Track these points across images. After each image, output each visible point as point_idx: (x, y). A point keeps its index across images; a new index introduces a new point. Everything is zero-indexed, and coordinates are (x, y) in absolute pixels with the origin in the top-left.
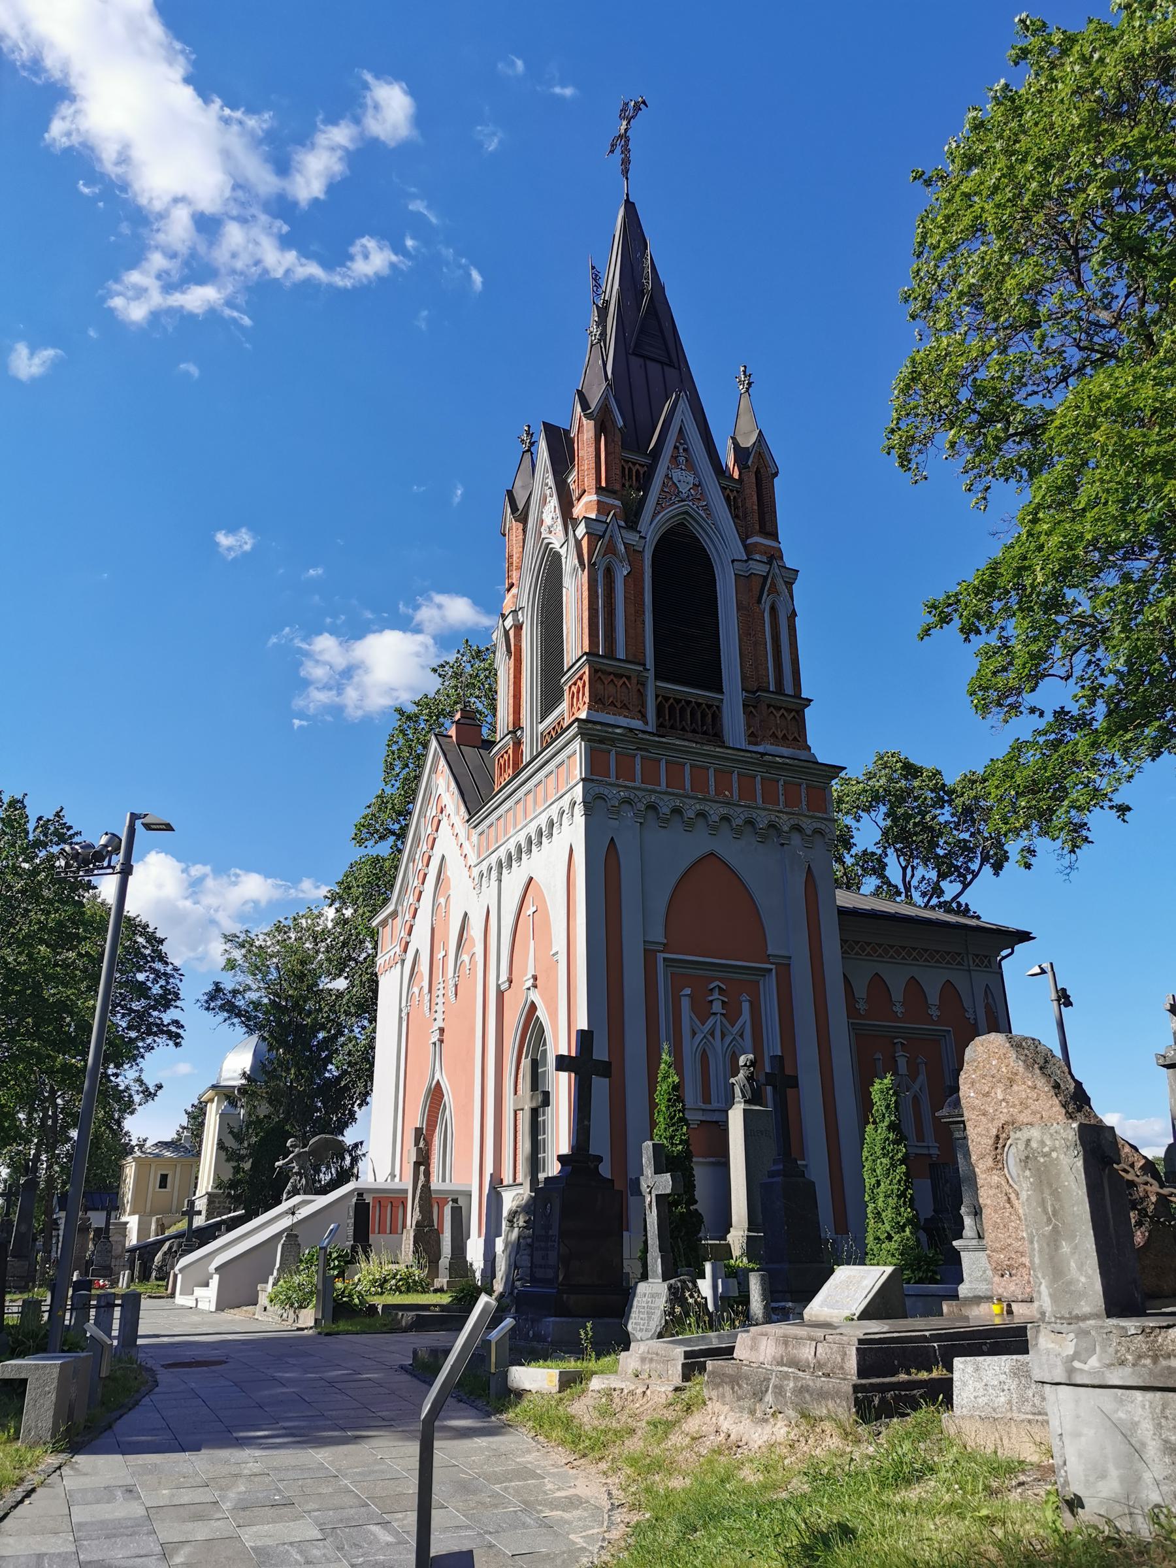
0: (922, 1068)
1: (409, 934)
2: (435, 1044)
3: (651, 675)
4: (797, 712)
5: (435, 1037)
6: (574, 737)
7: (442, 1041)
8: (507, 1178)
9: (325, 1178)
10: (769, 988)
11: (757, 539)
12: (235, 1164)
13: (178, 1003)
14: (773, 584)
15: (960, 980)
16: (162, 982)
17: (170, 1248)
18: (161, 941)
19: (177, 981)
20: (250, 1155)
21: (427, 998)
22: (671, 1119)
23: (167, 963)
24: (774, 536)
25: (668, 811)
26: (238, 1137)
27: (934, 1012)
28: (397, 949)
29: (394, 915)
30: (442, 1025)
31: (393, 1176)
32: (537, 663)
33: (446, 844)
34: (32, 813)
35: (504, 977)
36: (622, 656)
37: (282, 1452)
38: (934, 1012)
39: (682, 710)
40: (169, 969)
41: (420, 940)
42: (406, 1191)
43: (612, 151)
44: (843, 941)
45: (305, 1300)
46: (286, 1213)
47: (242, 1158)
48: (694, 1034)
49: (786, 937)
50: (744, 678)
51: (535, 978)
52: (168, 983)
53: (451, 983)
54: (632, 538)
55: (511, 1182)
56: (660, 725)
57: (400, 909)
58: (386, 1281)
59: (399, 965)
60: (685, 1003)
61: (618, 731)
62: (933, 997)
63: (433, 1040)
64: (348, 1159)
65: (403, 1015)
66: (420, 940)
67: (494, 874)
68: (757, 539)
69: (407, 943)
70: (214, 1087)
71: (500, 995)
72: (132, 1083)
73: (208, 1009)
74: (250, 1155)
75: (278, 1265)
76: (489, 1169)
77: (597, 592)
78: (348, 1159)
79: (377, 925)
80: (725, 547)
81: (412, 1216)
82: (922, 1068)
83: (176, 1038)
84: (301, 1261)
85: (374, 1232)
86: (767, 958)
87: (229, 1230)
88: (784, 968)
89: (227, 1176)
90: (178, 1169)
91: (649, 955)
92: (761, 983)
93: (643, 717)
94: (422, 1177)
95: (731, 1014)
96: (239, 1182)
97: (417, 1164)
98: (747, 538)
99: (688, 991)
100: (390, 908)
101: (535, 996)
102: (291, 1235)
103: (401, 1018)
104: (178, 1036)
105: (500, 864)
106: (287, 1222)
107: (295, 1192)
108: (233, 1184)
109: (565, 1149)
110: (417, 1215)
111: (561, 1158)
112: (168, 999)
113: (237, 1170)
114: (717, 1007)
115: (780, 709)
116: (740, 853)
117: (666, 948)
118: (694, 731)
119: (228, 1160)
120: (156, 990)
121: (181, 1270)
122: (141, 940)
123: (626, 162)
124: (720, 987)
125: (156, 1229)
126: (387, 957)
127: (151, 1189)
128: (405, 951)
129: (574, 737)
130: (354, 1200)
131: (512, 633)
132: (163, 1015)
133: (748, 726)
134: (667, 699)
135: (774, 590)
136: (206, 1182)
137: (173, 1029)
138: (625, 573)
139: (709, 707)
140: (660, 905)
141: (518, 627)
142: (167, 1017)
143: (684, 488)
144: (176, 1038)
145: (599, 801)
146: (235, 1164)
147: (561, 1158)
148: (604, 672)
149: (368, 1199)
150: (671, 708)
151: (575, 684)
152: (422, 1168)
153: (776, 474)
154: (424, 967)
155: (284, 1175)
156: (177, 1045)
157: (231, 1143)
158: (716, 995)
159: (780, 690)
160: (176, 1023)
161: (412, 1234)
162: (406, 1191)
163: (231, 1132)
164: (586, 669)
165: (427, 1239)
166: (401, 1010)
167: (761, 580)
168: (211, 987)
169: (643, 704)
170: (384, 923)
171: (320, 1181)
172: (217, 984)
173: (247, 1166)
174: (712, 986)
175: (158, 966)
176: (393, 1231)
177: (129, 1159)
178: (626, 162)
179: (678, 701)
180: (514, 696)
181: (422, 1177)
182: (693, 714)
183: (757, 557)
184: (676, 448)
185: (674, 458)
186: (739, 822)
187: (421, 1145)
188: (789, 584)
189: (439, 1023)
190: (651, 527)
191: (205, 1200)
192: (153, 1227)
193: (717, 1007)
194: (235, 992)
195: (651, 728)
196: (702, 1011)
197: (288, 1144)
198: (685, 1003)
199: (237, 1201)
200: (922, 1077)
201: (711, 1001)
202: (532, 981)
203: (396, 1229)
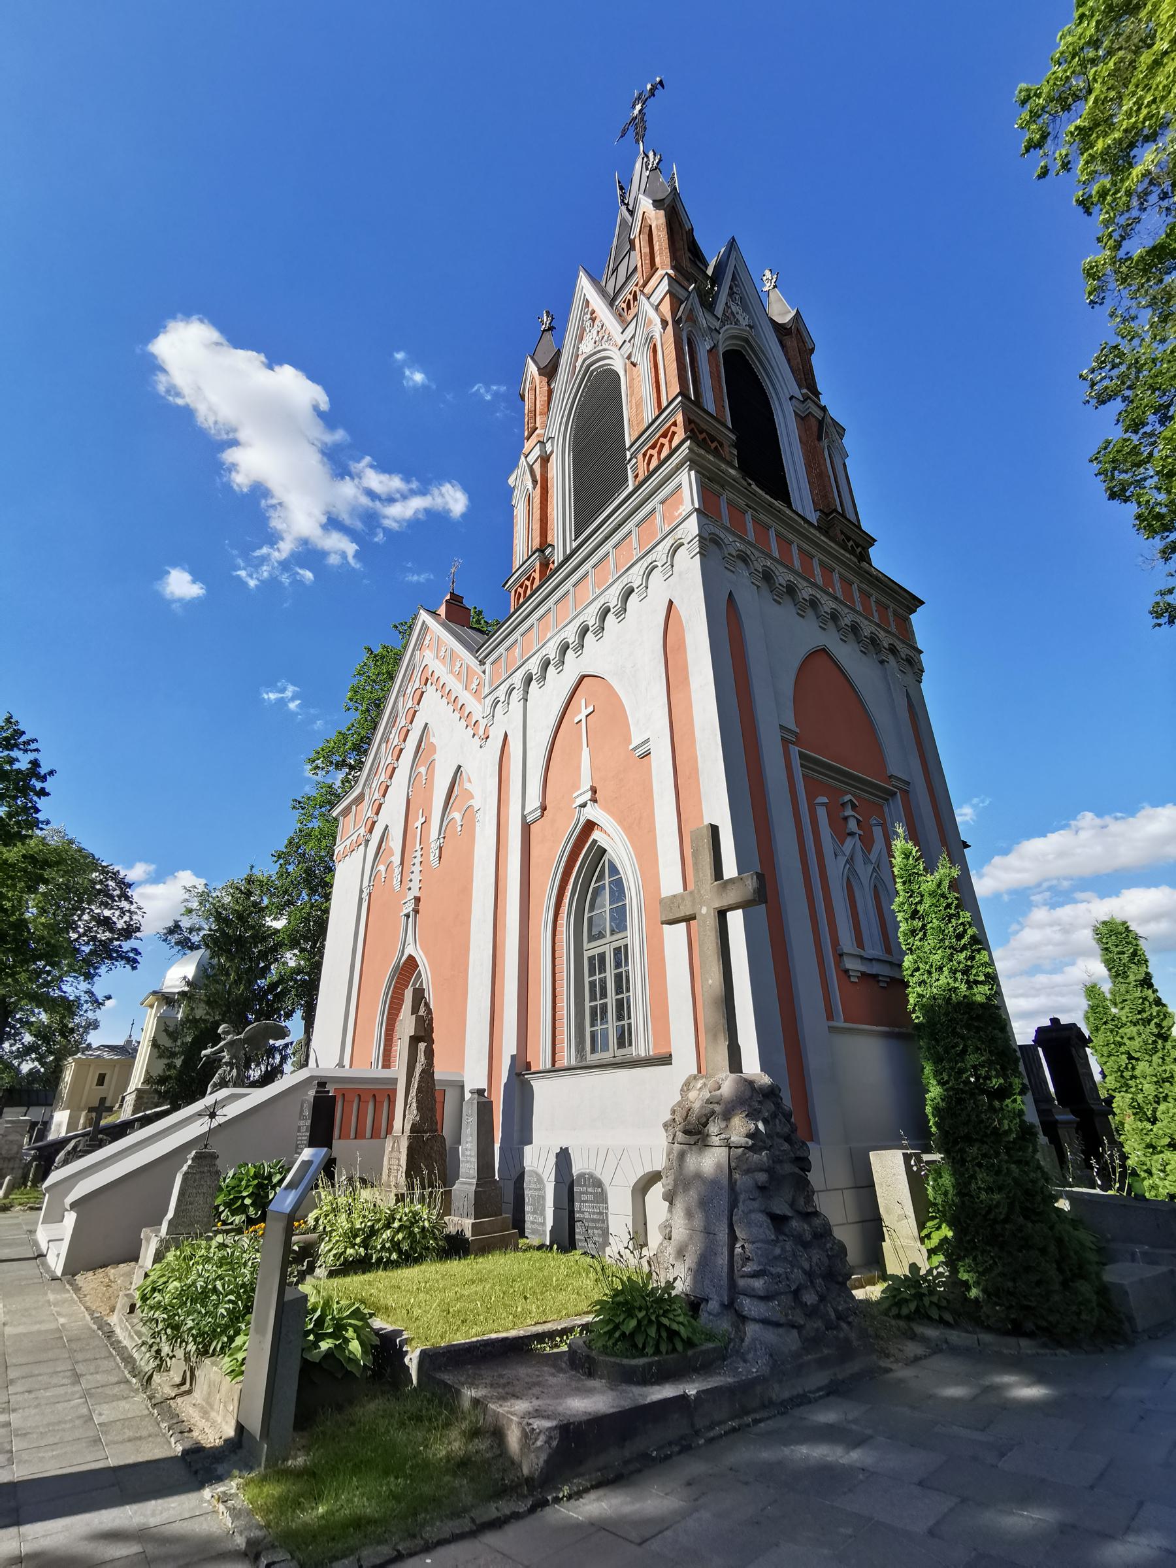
1: (377, 814)
2: (408, 916)
4: (863, 548)
5: (409, 908)
6: (678, 468)
7: (416, 912)
8: (541, 1058)
9: (255, 1073)
12: (166, 1061)
13: (138, 934)
16: (126, 918)
17: (75, 1148)
18: (129, 886)
19: (140, 918)
20: (182, 1053)
21: (397, 871)
22: (959, 937)
23: (131, 903)
26: (173, 1035)
28: (362, 831)
29: (360, 799)
30: (418, 895)
31: (341, 1065)
32: (569, 484)
34: (41, 803)
35: (534, 802)
40: (133, 908)
41: (392, 814)
42: (395, 1081)
45: (214, 1335)
46: (200, 1114)
47: (173, 1055)
51: (594, 790)
52: (131, 919)
53: (434, 846)
55: (549, 1066)
57: (367, 791)
58: (373, 1232)
59: (362, 848)
60: (822, 813)
63: (405, 912)
64: (278, 1057)
65: (365, 896)
66: (392, 814)
67: (517, 695)
69: (374, 823)
70: (155, 993)
71: (526, 827)
72: (82, 994)
73: (165, 940)
74: (182, 1053)
75: (170, 1214)
76: (509, 1047)
77: (682, 349)
78: (278, 1057)
79: (339, 814)
81: (403, 1118)
83: (133, 963)
84: (221, 1189)
85: (343, 1136)
87: (142, 1127)
89: (158, 1071)
90: (117, 1069)
92: (886, 808)
94: (421, 1057)
96: (169, 1077)
97: (415, 1040)
100: (357, 792)
101: (592, 813)
102: (204, 1157)
103: (361, 899)
104: (135, 961)
105: (528, 680)
106: (200, 1127)
107: (223, 1084)
108: (162, 1080)
110: (413, 1115)
112: (129, 931)
113: (170, 1066)
114: (852, 825)
116: (846, 654)
119: (160, 1057)
120: (120, 924)
121: (47, 1189)
122: (111, 883)
125: (85, 1123)
126: (348, 843)
127: (87, 1088)
128: (371, 831)
129: (678, 468)
130: (312, 1093)
131: (537, 468)
132: (123, 944)
136: (137, 1079)
137: (131, 955)
138: (708, 348)
140: (787, 684)
141: (545, 459)
142: (126, 946)
144: (133, 963)
146: (166, 1061)
149: (331, 1089)
152: (422, 1046)
153: (812, 351)
154: (395, 843)
155: (213, 1064)
156: (134, 968)
157: (166, 1042)
158: (849, 812)
160: (135, 950)
161: (404, 1144)
162: (395, 1081)
163: (166, 1030)
164: (680, 418)
165: (429, 1156)
166: (361, 891)
168: (171, 924)
170: (346, 812)
171: (248, 1078)
172: (176, 922)
173: (178, 1062)
175: (124, 904)
176: (375, 1134)
177: (70, 1059)
180: (541, 520)
181: (421, 1057)
187: (422, 1012)
189: (416, 892)
191: (134, 1096)
192: (82, 1121)
194: (191, 930)
197: (220, 1031)
198: (822, 813)
199: (163, 1097)
202: (590, 793)
203: (381, 1130)
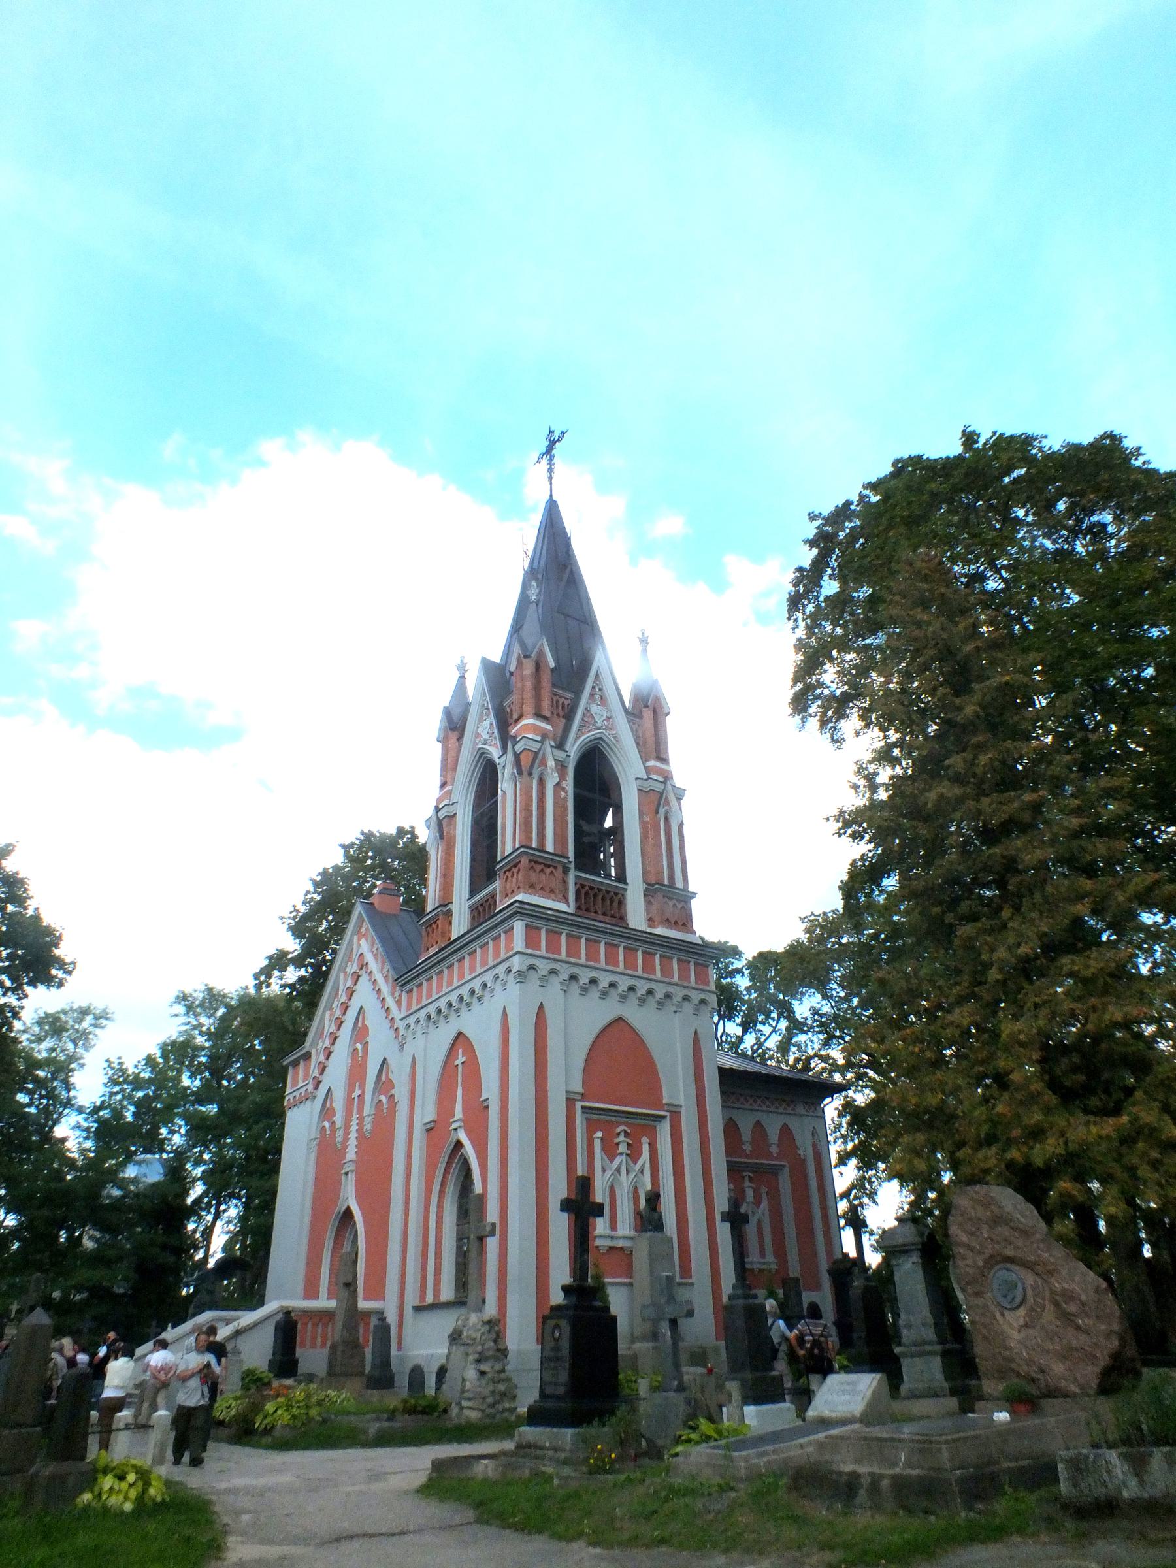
0: (765, 1197)
3: (572, 866)
10: (664, 1132)
11: (652, 763)
14: (667, 799)
15: (794, 1124)
24: (665, 760)
25: (587, 981)
27: (774, 1150)
33: (364, 996)
36: (534, 846)
37: (921, 1401)
38: (774, 1150)
39: (595, 896)
43: (539, 461)
44: (722, 1093)
48: (604, 1171)
49: (677, 1087)
50: (645, 872)
54: (561, 755)
56: (578, 908)
60: (598, 1145)
61: (550, 912)
62: (773, 1136)
68: (652, 763)
80: (629, 769)
82: (765, 1197)
86: (661, 1107)
88: (675, 1115)
91: (570, 1102)
93: (566, 900)
95: (634, 1155)
98: (647, 761)
99: (599, 1134)
109: (567, 1279)
111: (565, 1289)
114: (623, 1148)
115: (671, 898)
116: (642, 1018)
117: (583, 1097)
118: (604, 914)
123: (551, 471)
124: (625, 1132)
133: (648, 911)
134: (583, 886)
135: (667, 802)
139: (616, 894)
143: (599, 721)
145: (532, 971)
147: (565, 1289)
148: (536, 862)
150: (587, 894)
151: (509, 870)
158: (622, 1137)
159: (672, 884)
167: (657, 796)
169: (566, 889)
174: (618, 1130)
178: (551, 471)
179: (592, 888)
182: (603, 899)
183: (654, 777)
184: (593, 687)
185: (592, 695)
186: (679, 998)
188: (679, 799)
190: (574, 748)
193: (623, 1148)
195: (571, 910)
196: (610, 1151)
198: (598, 1145)
200: (764, 1205)
201: (618, 1144)
